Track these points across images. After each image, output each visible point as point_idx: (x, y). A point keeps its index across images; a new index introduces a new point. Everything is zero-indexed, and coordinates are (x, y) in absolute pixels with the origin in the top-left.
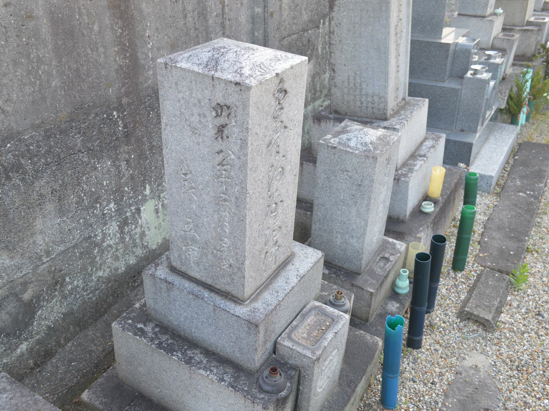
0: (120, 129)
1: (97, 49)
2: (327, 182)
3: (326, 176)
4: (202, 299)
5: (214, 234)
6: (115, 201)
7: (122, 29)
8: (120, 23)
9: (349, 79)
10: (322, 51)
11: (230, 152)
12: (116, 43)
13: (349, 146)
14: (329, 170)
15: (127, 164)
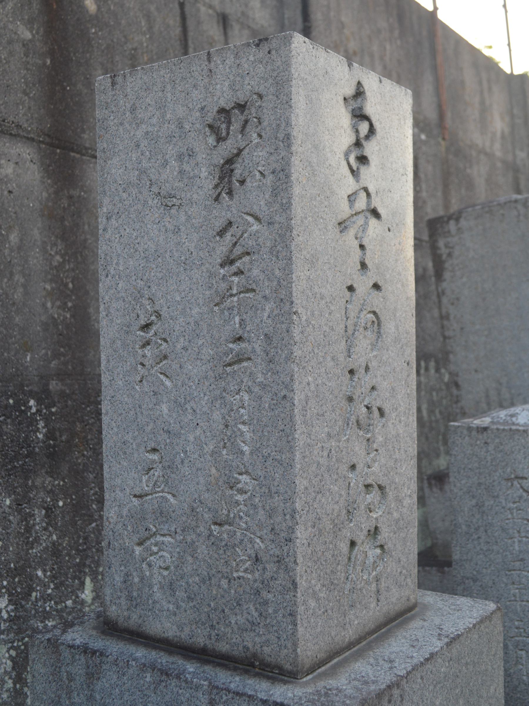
0: (40, 436)
1: (12, 274)
2: (478, 516)
3: (474, 502)
4: (178, 677)
5: (214, 471)
6: (10, 595)
7: (62, 256)
8: (61, 246)
9: (487, 396)
10: (429, 416)
11: (250, 219)
12: (49, 277)
13: (518, 424)
14: (480, 484)
15: (47, 516)
